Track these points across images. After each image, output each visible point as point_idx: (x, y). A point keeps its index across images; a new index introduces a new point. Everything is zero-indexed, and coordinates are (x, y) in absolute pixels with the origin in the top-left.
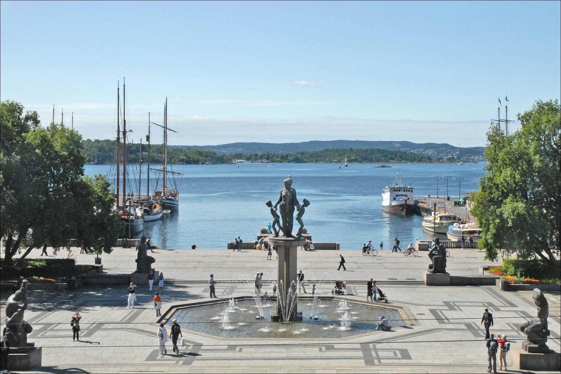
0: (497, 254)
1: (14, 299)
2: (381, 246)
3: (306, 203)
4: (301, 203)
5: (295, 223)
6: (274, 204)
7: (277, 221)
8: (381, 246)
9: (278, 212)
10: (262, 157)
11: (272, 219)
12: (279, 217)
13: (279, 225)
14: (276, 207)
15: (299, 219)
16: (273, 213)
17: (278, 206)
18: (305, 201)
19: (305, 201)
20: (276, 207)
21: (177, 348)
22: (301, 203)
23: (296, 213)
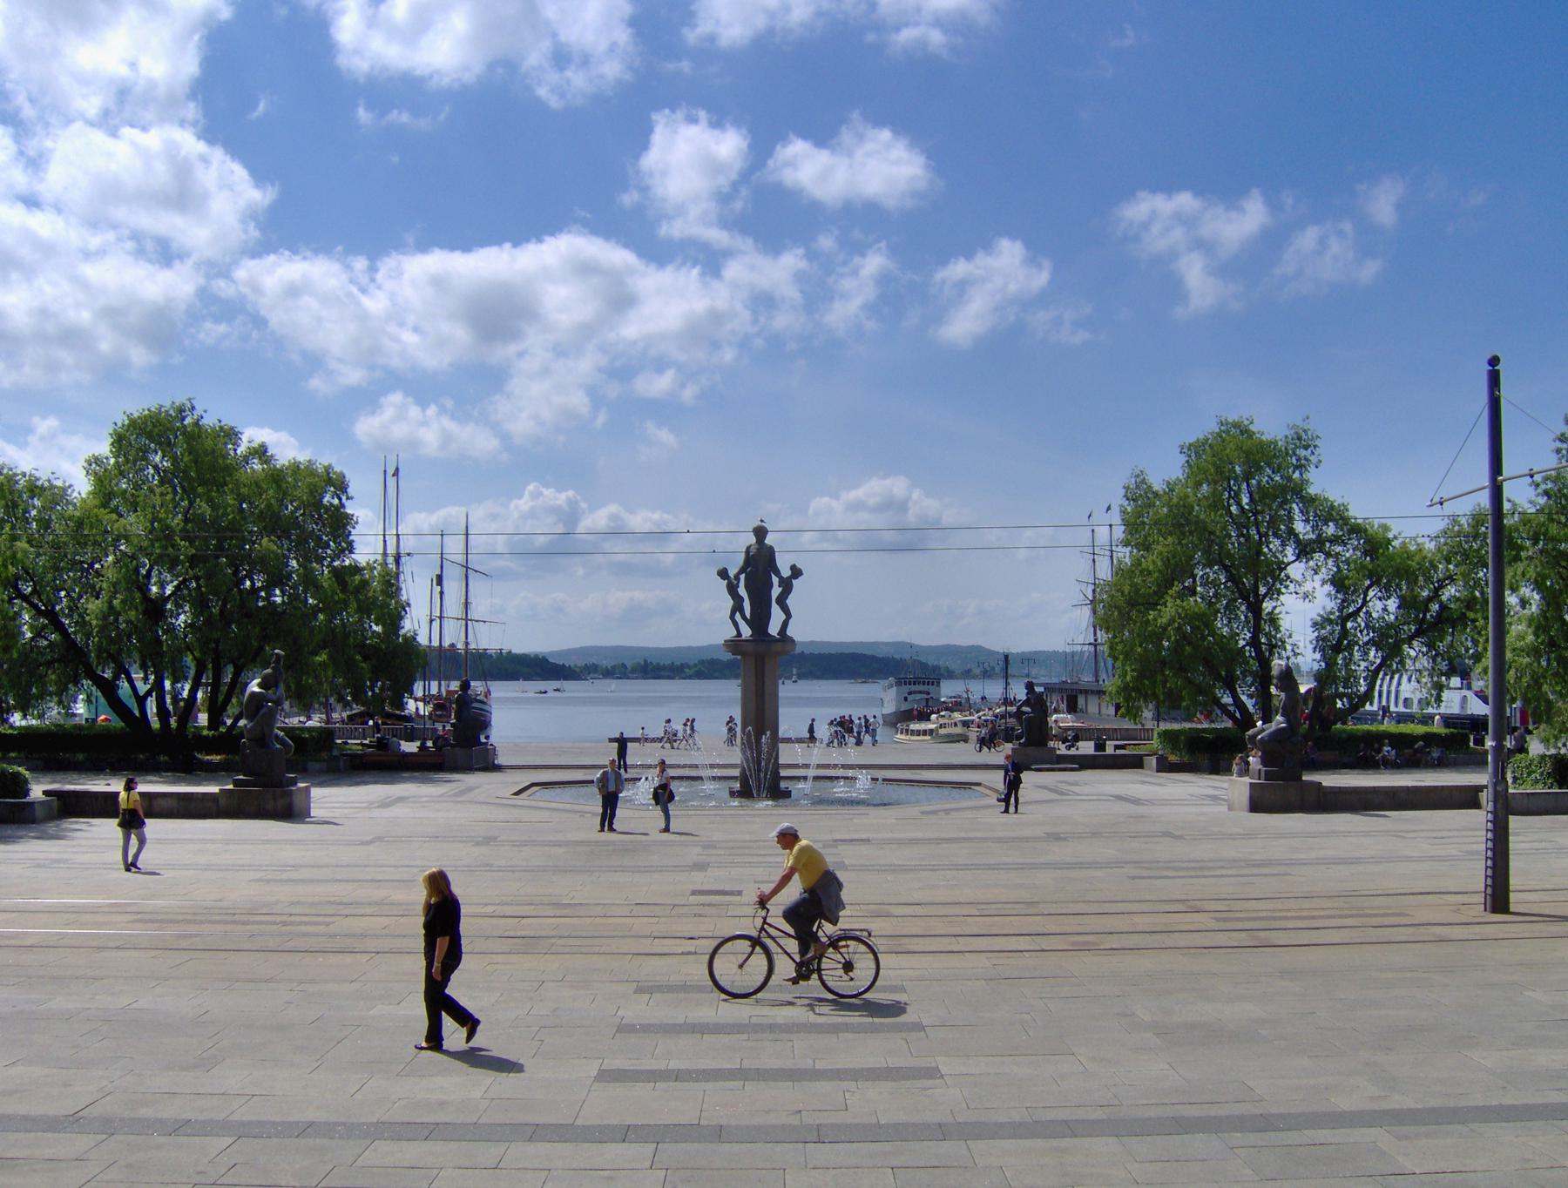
0: (1282, 566)
1: (259, 685)
2: (1109, 508)
3: (796, 572)
4: (786, 573)
5: (776, 612)
6: (732, 574)
7: (738, 607)
8: (1109, 508)
9: (742, 591)
10: (633, 671)
11: (729, 603)
12: (742, 599)
13: (743, 617)
14: (737, 577)
15: (782, 601)
16: (732, 589)
17: (742, 577)
18: (793, 568)
19: (793, 568)
20: (737, 577)
21: (604, 798)
22: (786, 573)
23: (776, 591)
